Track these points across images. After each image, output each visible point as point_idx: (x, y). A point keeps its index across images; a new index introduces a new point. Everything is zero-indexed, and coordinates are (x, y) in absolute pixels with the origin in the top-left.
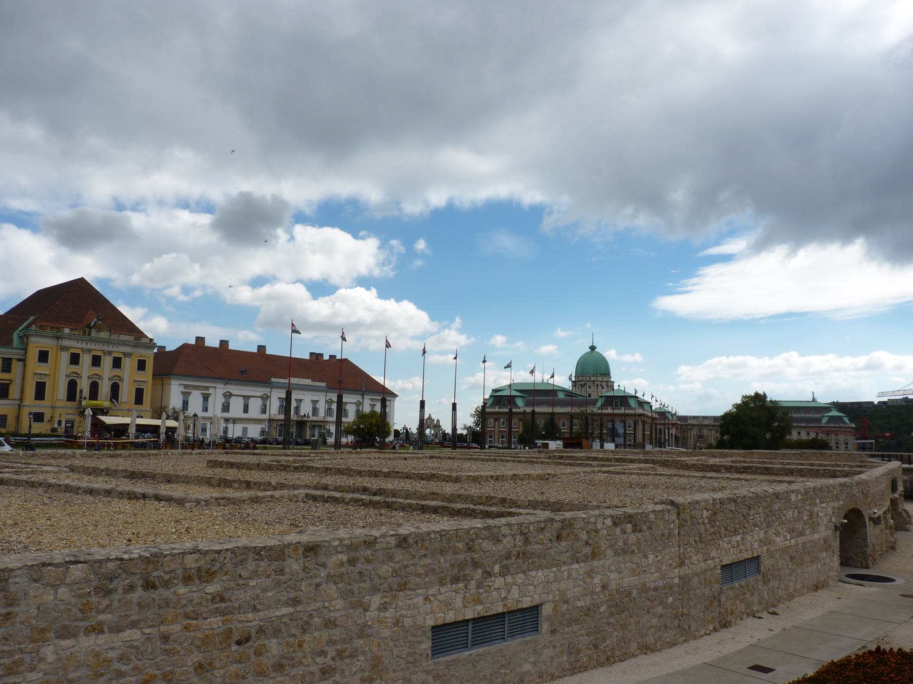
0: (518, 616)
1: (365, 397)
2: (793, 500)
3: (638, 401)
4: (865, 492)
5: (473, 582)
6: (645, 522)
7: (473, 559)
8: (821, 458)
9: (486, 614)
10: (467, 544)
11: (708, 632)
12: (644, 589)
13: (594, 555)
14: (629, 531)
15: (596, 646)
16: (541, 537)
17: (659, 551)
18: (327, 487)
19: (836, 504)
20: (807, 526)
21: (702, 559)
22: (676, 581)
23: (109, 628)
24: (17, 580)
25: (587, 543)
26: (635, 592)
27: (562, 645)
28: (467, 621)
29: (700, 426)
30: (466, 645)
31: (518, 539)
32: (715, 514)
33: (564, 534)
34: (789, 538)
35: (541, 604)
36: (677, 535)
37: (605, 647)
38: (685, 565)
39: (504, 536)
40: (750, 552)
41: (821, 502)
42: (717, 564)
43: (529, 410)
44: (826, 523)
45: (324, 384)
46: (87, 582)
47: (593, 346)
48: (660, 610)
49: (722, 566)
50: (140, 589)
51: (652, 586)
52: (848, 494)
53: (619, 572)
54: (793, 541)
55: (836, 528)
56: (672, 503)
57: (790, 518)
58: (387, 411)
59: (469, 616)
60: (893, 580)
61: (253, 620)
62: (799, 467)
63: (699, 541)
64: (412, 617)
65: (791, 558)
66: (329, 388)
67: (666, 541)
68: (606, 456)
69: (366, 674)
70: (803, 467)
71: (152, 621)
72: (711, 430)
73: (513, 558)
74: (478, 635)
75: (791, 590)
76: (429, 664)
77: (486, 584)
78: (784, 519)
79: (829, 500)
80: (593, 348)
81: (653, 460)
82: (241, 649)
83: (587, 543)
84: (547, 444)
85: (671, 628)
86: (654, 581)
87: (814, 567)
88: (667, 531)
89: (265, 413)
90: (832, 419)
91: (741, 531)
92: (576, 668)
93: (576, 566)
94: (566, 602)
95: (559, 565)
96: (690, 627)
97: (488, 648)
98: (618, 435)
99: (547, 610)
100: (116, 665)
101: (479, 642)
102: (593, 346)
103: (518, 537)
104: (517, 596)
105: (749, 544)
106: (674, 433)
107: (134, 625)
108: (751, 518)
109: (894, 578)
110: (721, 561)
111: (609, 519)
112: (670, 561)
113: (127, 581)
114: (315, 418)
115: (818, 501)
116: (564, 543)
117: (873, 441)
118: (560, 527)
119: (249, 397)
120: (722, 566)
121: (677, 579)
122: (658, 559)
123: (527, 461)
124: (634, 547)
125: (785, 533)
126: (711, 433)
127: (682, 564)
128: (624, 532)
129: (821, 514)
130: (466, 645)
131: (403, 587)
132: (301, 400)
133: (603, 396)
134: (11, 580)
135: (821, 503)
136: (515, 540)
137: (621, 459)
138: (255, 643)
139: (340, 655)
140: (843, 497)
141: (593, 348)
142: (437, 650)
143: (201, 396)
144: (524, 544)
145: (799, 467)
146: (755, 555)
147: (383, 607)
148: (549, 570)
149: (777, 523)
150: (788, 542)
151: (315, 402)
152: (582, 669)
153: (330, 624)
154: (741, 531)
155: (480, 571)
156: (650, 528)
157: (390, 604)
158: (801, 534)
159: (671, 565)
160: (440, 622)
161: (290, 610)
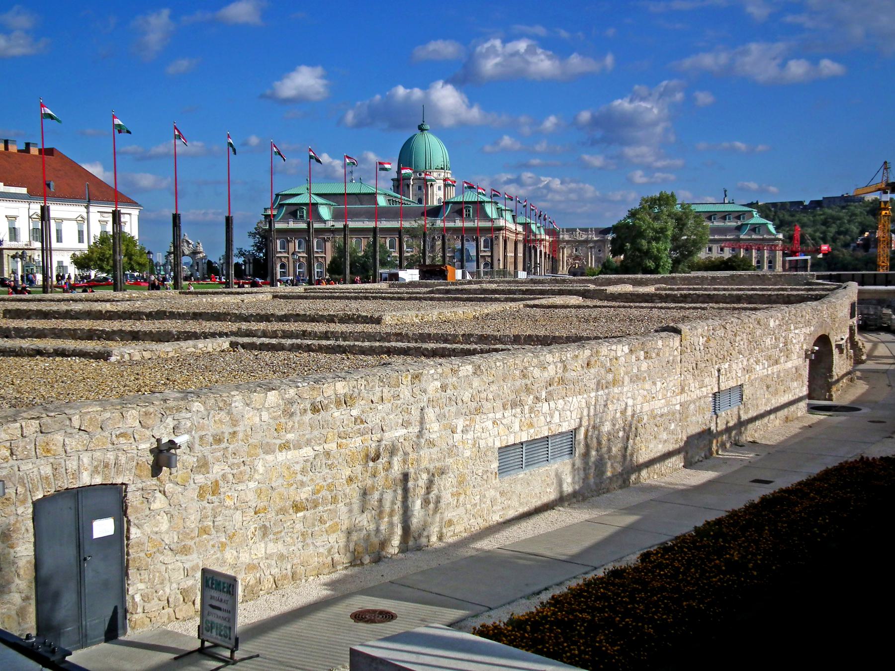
0: (557, 440)
1: (92, 209)
2: (771, 326)
4: (833, 316)
5: (527, 407)
6: (654, 349)
7: (526, 385)
8: (758, 282)
9: (536, 437)
10: (522, 371)
11: (701, 459)
13: (615, 382)
14: (642, 358)
16: (576, 365)
17: (665, 379)
19: (807, 330)
20: (782, 354)
21: (698, 387)
22: (678, 407)
23: (294, 446)
24: (237, 404)
31: (559, 367)
32: (708, 340)
33: (593, 360)
34: (766, 367)
36: (679, 362)
40: (735, 380)
41: (796, 328)
42: (709, 392)
43: (339, 225)
44: (798, 350)
45: (24, 191)
46: (277, 407)
48: (664, 436)
50: (309, 412)
51: (659, 413)
52: (818, 319)
54: (769, 369)
55: (807, 356)
57: (768, 345)
59: (524, 439)
60: (859, 410)
63: (695, 368)
65: (768, 387)
66: (31, 196)
67: (671, 367)
69: (455, 490)
71: (320, 440)
73: (555, 384)
74: (540, 451)
76: (496, 482)
77: (536, 409)
78: (763, 346)
79: (802, 325)
84: (397, 275)
86: (660, 408)
88: (671, 358)
89: (83, 242)
91: (729, 359)
92: (600, 489)
98: (469, 259)
100: (299, 477)
101: (532, 463)
103: (559, 365)
104: (559, 421)
105: (734, 372)
107: (308, 443)
108: (737, 345)
109: (859, 407)
110: (712, 389)
112: (673, 388)
113: (302, 405)
114: (14, 244)
115: (792, 328)
116: (592, 371)
117: (809, 257)
118: (590, 354)
119: (62, 220)
121: (679, 405)
122: (664, 385)
123: (410, 298)
124: (645, 375)
125: (764, 361)
127: (683, 391)
128: (638, 359)
129: (794, 341)
131: (478, 411)
132: (15, 218)
134: (233, 405)
135: (795, 329)
136: (556, 367)
140: (814, 322)
142: (503, 470)
144: (563, 371)
146: (739, 384)
148: (582, 396)
149: (757, 351)
150: (765, 370)
151: (11, 219)
152: (605, 490)
154: (729, 359)
155: (532, 397)
156: (658, 355)
157: (470, 426)
158: (777, 362)
159: (674, 392)
161: (404, 431)
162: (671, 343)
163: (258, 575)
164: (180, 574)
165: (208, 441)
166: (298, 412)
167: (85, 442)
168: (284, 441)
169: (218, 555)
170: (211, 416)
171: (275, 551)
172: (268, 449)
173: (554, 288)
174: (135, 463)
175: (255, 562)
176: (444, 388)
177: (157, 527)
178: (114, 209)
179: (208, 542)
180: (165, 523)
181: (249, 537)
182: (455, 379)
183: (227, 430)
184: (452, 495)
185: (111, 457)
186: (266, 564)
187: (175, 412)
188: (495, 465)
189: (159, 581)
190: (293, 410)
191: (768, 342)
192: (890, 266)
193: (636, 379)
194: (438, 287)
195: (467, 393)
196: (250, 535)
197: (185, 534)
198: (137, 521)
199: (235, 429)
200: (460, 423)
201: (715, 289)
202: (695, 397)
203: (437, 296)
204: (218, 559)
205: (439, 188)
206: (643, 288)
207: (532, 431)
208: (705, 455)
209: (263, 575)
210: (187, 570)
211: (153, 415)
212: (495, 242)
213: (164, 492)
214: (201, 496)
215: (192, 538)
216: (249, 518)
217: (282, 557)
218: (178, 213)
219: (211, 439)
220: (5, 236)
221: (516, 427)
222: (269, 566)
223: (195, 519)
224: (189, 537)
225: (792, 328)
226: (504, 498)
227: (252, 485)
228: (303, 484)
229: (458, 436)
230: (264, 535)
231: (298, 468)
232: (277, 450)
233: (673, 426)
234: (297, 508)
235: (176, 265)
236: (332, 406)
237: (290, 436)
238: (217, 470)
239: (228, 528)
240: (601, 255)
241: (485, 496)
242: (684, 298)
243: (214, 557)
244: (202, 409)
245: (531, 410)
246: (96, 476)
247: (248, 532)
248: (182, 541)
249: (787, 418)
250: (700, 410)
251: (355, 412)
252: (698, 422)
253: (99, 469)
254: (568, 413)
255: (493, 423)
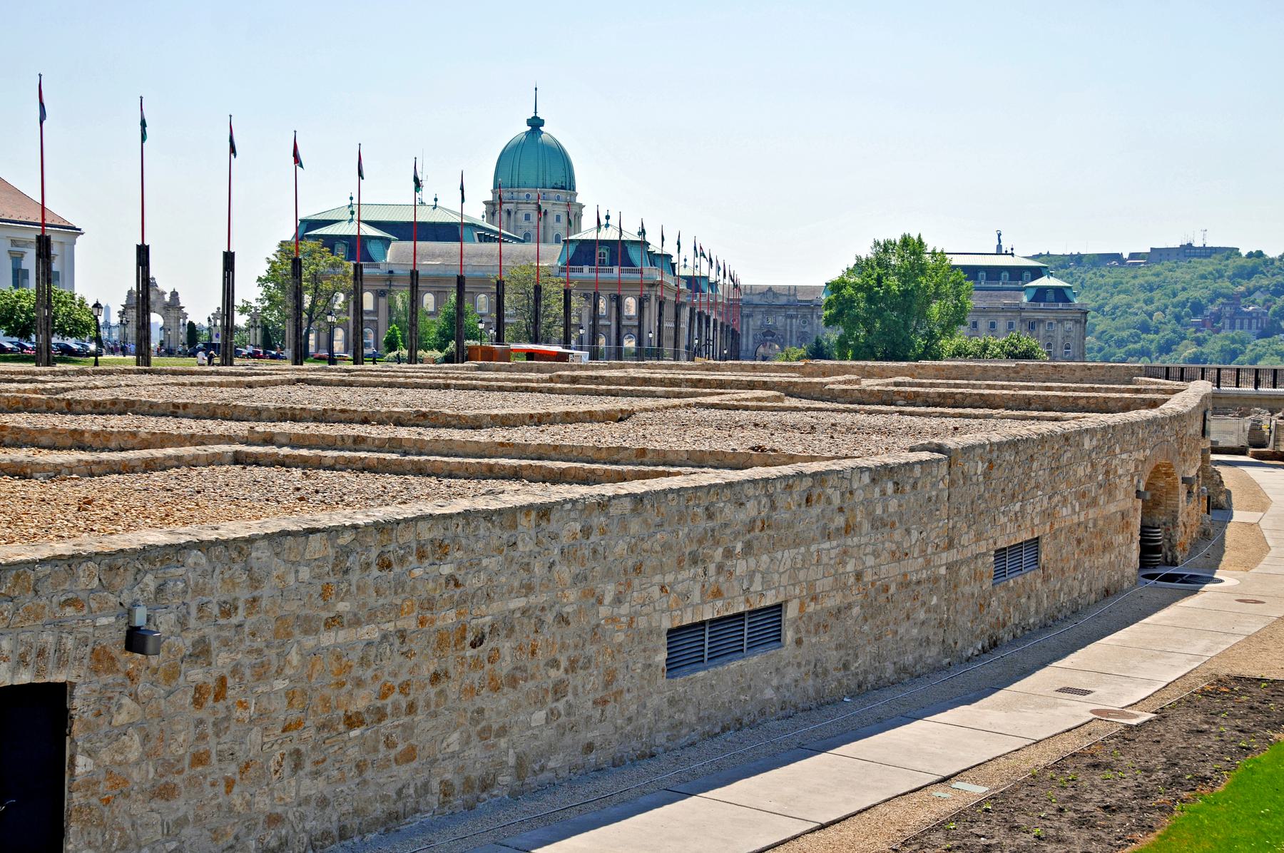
3: (649, 253)
9: (726, 614)
12: (904, 584)
13: (849, 529)
15: (846, 667)
18: (272, 439)
22: (943, 571)
25: (841, 510)
26: (893, 589)
27: (808, 663)
28: (703, 623)
29: (771, 308)
30: (701, 659)
35: (786, 602)
37: (857, 668)
38: (953, 547)
39: (749, 498)
41: (1123, 451)
47: (535, 118)
48: (922, 615)
49: (996, 551)
53: (876, 554)
56: (940, 449)
58: (152, 274)
59: (708, 617)
61: (485, 616)
62: (1041, 393)
64: (647, 615)
65: (1079, 542)
68: (670, 376)
70: (993, 392)
72: (791, 317)
75: (1076, 595)
80: (536, 123)
81: (765, 383)
82: (474, 651)
83: (841, 510)
85: (934, 644)
87: (1106, 559)
88: (934, 493)
90: (1041, 293)
93: (826, 545)
94: (814, 599)
95: (808, 542)
96: (956, 643)
97: (741, 662)
99: (791, 612)
102: (535, 118)
106: (719, 320)
107: (372, 617)
110: (995, 544)
111: (867, 473)
115: (1118, 451)
120: (996, 551)
121: (944, 567)
125: (1074, 502)
126: (791, 325)
127: (950, 545)
128: (883, 493)
129: (1120, 471)
130: (701, 659)
133: (572, 241)
136: (759, 503)
137: (700, 380)
138: (488, 645)
139: (573, 666)
141: (536, 123)
143: (8, 257)
145: (1041, 393)
147: (618, 600)
153: (563, 620)
155: (720, 550)
156: (914, 486)
158: (1094, 503)
159: (938, 546)
160: (677, 624)
162: (935, 473)
163: (284, 832)
164: (156, 832)
165: (211, 613)
166: (357, 568)
167: (6, 614)
168: (332, 615)
169: (220, 800)
170: (217, 571)
171: (313, 792)
172: (308, 625)
173: (741, 378)
174: (89, 649)
175: (279, 810)
176: (586, 532)
177: (122, 753)
178: (39, 233)
179: (205, 778)
180: (135, 746)
181: (272, 770)
182: (602, 519)
183: (243, 595)
184: (595, 703)
185: (49, 638)
186: (297, 814)
187: (158, 564)
188: (662, 657)
189: (119, 844)
190: (348, 564)
191: (1081, 472)
192: (423, 440)
193: (879, 524)
194: (560, 373)
195: (621, 542)
196: (273, 765)
197: (171, 766)
198: (89, 745)
199: (256, 593)
200: (610, 591)
201: (989, 387)
202: (969, 555)
203: (559, 385)
204: (219, 806)
205: (527, 217)
206: (293, 431)
207: (719, 603)
208: (983, 647)
209: (291, 832)
210: (168, 824)
211: (122, 570)
212: (646, 304)
213: (136, 695)
214: (198, 702)
215: (180, 772)
216: (272, 738)
217: (323, 802)
218: (232, 250)
219: (216, 611)
220: (6, 285)
221: (696, 597)
222: (302, 818)
223: (184, 741)
224: (174, 770)
225: (1118, 451)
226: (674, 710)
227: (280, 685)
228: (359, 683)
229: (604, 611)
230: (296, 765)
231: (355, 657)
232: (322, 628)
233: (934, 600)
234: (352, 721)
235: (144, 326)
236: (411, 558)
237: (343, 607)
238: (222, 660)
239: (238, 754)
240: (806, 329)
241: (645, 706)
242: (942, 400)
243: (214, 802)
244: (204, 560)
245: (720, 568)
246: (22, 669)
247: (271, 762)
248: (162, 776)
249: (1107, 591)
250: (977, 576)
251: (446, 569)
252: (973, 595)
253: (28, 659)
254: (776, 577)
255: (661, 590)
